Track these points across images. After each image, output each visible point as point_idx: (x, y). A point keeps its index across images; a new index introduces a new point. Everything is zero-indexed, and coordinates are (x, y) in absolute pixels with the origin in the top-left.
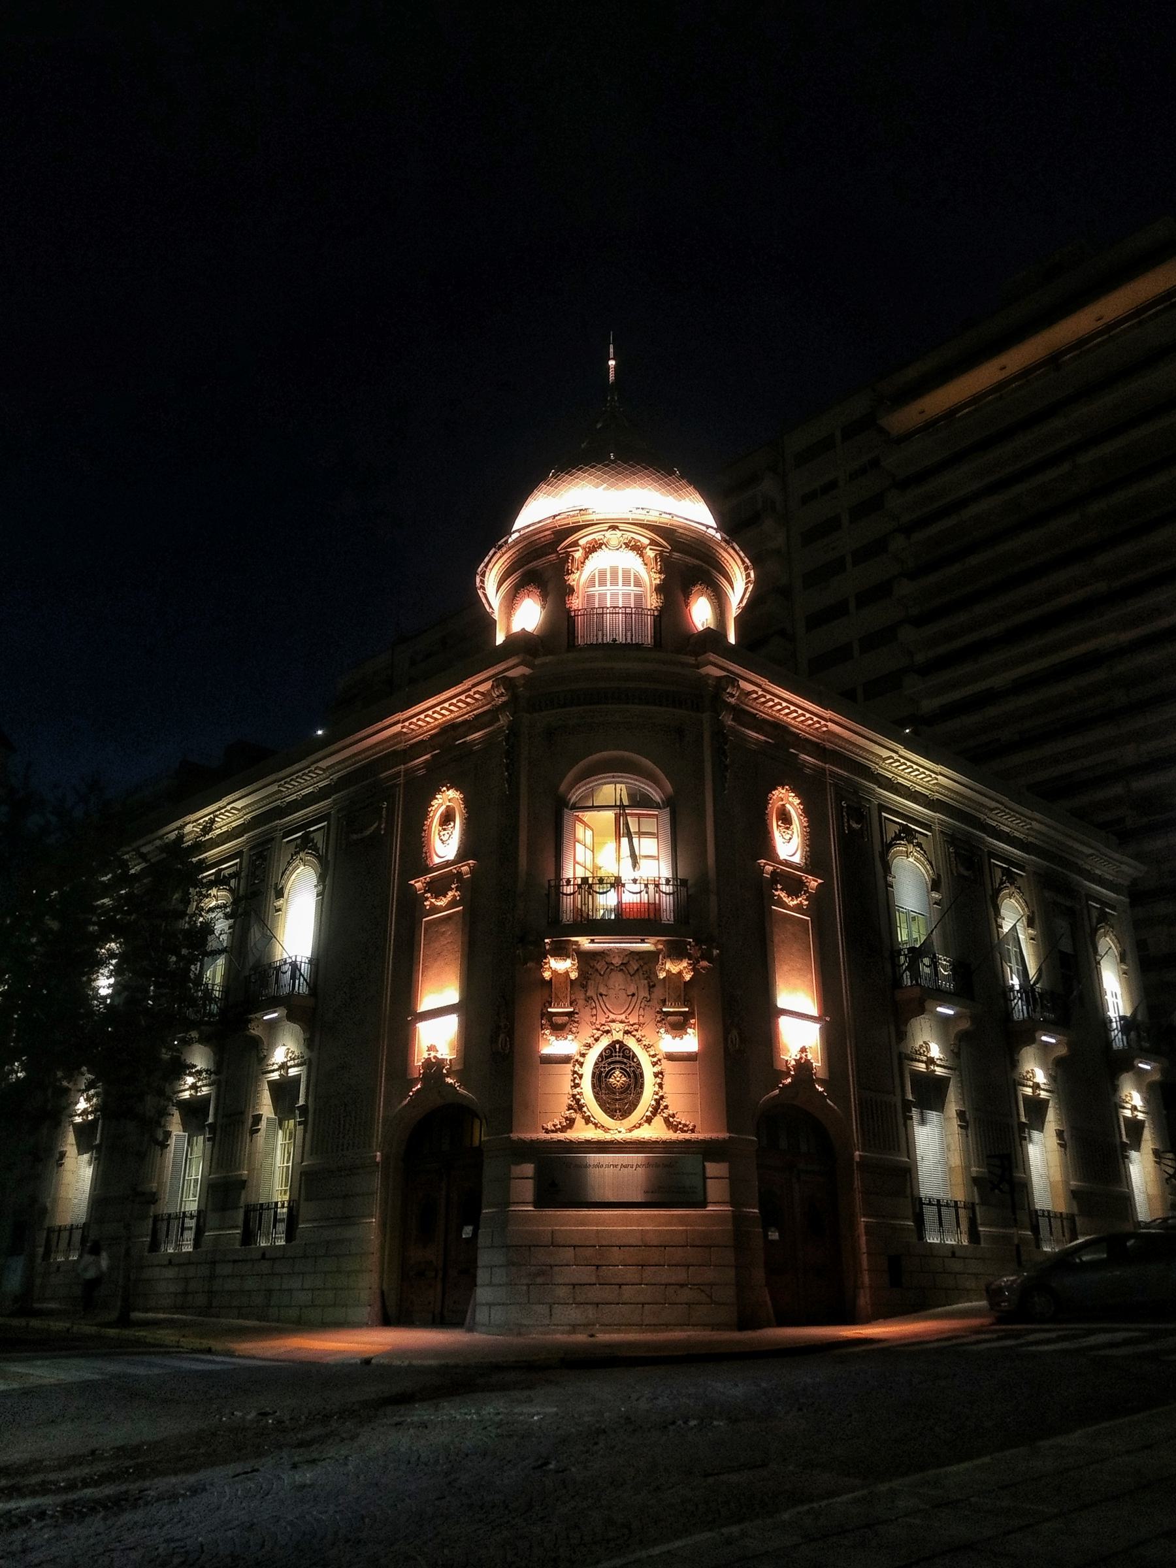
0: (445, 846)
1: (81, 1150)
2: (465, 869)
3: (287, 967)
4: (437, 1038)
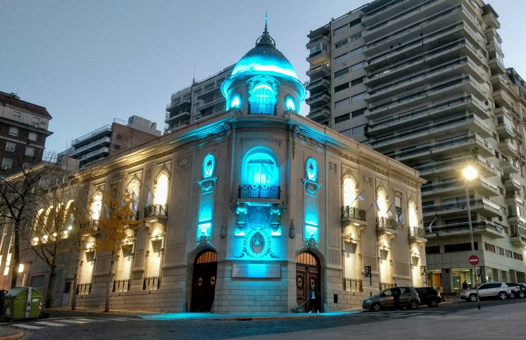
0: (208, 172)
1: (88, 260)
2: (214, 180)
3: (158, 207)
4: (204, 229)
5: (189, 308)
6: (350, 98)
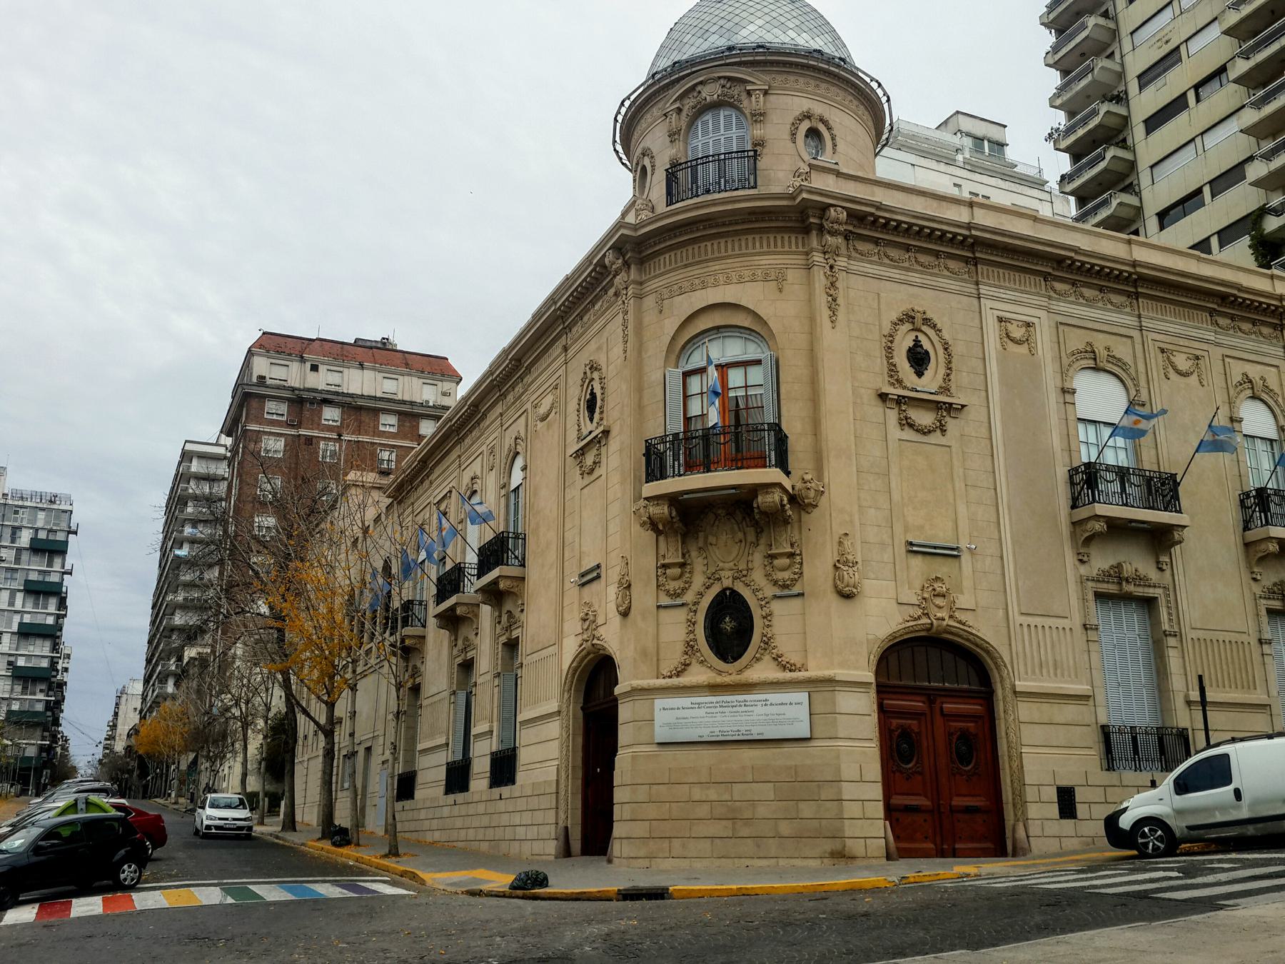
5: (576, 845)
6: (1198, 140)
